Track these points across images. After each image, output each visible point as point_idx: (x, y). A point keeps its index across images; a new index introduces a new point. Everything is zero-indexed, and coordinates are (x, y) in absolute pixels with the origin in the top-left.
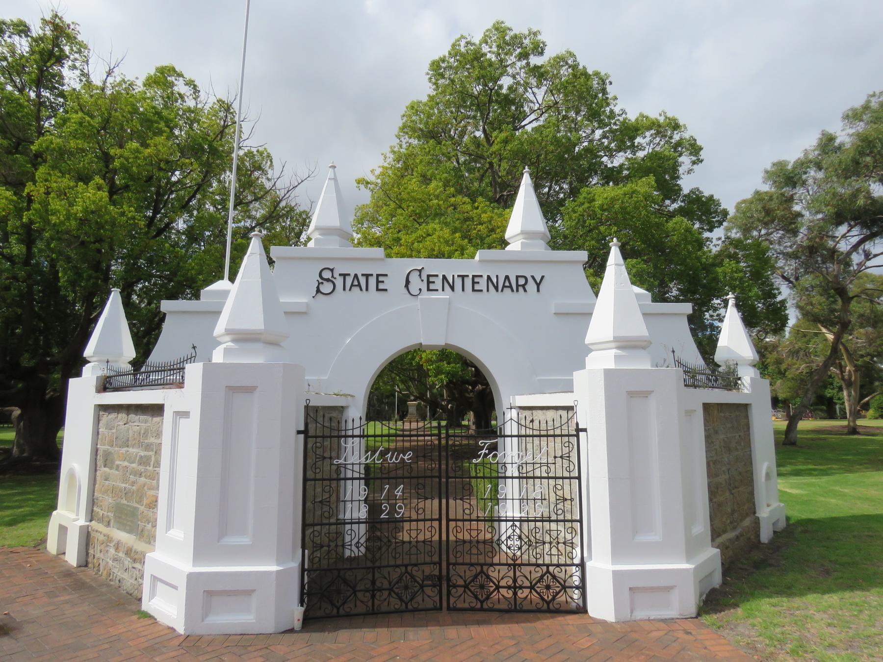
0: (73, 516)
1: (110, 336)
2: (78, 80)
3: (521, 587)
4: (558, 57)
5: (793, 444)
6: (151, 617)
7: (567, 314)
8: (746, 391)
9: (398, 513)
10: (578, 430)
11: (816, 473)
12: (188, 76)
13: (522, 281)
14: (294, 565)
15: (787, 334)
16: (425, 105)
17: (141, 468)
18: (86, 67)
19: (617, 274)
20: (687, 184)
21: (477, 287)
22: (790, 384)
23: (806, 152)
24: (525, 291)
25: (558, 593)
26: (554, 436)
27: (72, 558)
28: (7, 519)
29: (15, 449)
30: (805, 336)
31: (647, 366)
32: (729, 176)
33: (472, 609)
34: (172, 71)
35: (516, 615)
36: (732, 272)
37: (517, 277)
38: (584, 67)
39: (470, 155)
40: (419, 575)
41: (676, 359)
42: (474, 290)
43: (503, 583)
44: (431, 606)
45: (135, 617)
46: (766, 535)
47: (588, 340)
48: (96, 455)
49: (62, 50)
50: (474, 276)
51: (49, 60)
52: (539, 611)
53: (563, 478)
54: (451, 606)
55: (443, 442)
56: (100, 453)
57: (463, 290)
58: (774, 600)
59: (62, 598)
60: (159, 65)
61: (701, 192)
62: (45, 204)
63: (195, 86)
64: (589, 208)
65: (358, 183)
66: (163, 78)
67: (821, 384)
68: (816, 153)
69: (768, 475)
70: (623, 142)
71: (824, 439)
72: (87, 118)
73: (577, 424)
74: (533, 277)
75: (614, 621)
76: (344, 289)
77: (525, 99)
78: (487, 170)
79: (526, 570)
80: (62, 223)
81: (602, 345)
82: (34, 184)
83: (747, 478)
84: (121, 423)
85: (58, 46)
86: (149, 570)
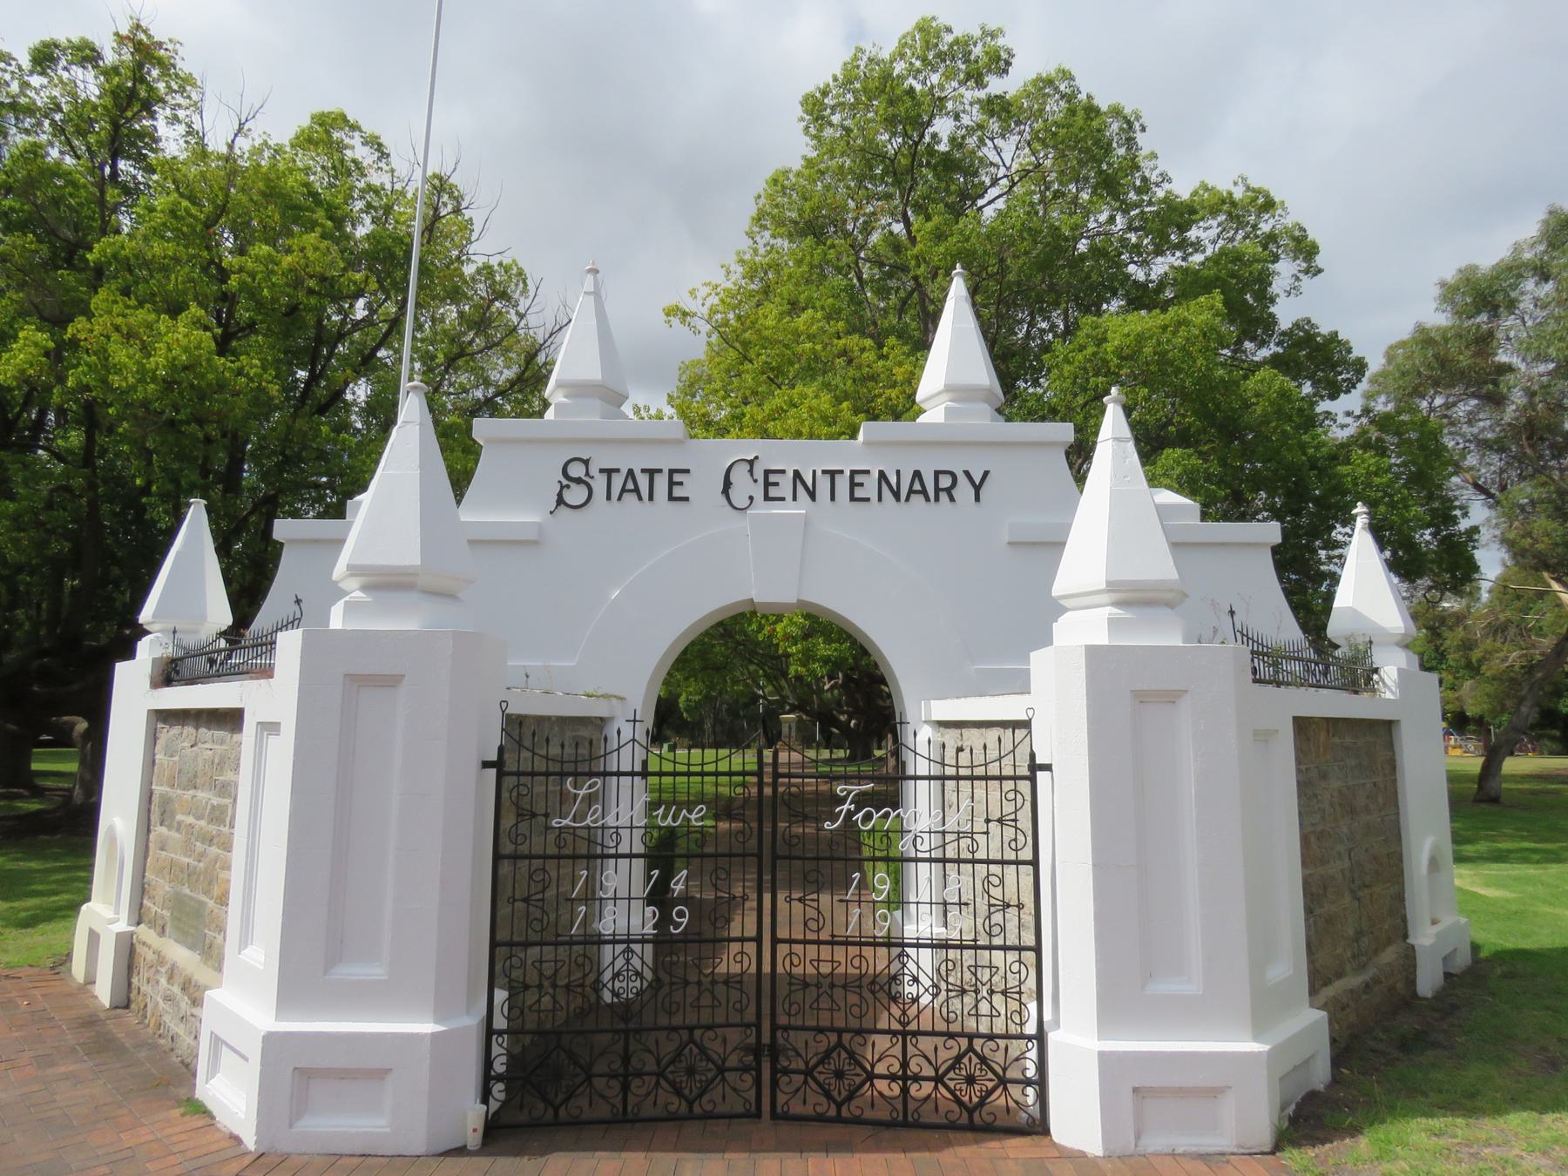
0: (111, 915)
1: (187, 586)
2: (181, 142)
3: (917, 1078)
4: (1039, 79)
5: (1495, 800)
6: (204, 1112)
7: (1034, 544)
8: (1388, 695)
9: (677, 925)
10: (1034, 767)
11: (1536, 857)
12: (368, 128)
13: (945, 482)
14: (471, 1021)
15: (1485, 596)
16: (798, 174)
17: (213, 828)
18: (196, 118)
19: (1118, 458)
20: (1286, 313)
21: (859, 493)
22: (1489, 688)
23: (1517, 248)
24: (952, 499)
25: (990, 1092)
26: (986, 778)
27: (103, 992)
28: (23, 914)
29: (77, 790)
30: (1518, 597)
31: (1177, 641)
32: (1373, 295)
33: (821, 1119)
34: (341, 120)
35: (904, 1133)
36: (1369, 474)
37: (937, 473)
38: (1089, 97)
39: (882, 265)
40: (715, 1047)
41: (1238, 627)
42: (853, 498)
43: (880, 1069)
44: (740, 1109)
45: (176, 1113)
46: (1428, 981)
47: (1058, 589)
48: (150, 802)
49: (151, 89)
50: (853, 473)
51: (129, 105)
52: (953, 1126)
53: (1003, 862)
54: (779, 1110)
55: (768, 791)
56: (155, 798)
57: (833, 498)
58: (1436, 1123)
59: (62, 1069)
60: (317, 109)
61: (1313, 326)
62: (103, 354)
63: (380, 145)
64: (1094, 354)
65: (668, 315)
66: (325, 132)
67: (1548, 688)
68: (1542, 248)
69: (1434, 863)
70: (1164, 237)
71: (1556, 792)
72: (185, 203)
73: (1032, 756)
74: (967, 473)
75: (1100, 1153)
76: (609, 498)
77: (981, 160)
78: (911, 293)
79: (926, 1044)
80: (133, 388)
81: (1085, 599)
82: (89, 319)
83: (1387, 866)
84: (186, 744)
85: (143, 80)
86: (210, 1021)
